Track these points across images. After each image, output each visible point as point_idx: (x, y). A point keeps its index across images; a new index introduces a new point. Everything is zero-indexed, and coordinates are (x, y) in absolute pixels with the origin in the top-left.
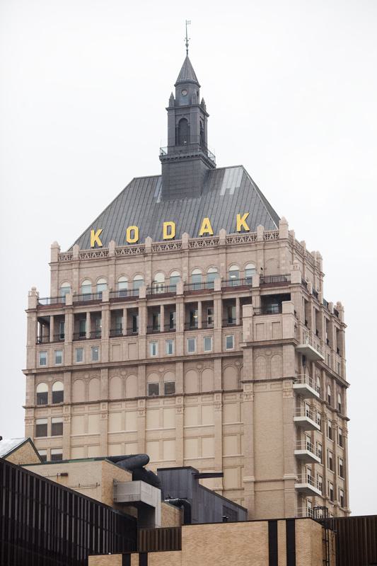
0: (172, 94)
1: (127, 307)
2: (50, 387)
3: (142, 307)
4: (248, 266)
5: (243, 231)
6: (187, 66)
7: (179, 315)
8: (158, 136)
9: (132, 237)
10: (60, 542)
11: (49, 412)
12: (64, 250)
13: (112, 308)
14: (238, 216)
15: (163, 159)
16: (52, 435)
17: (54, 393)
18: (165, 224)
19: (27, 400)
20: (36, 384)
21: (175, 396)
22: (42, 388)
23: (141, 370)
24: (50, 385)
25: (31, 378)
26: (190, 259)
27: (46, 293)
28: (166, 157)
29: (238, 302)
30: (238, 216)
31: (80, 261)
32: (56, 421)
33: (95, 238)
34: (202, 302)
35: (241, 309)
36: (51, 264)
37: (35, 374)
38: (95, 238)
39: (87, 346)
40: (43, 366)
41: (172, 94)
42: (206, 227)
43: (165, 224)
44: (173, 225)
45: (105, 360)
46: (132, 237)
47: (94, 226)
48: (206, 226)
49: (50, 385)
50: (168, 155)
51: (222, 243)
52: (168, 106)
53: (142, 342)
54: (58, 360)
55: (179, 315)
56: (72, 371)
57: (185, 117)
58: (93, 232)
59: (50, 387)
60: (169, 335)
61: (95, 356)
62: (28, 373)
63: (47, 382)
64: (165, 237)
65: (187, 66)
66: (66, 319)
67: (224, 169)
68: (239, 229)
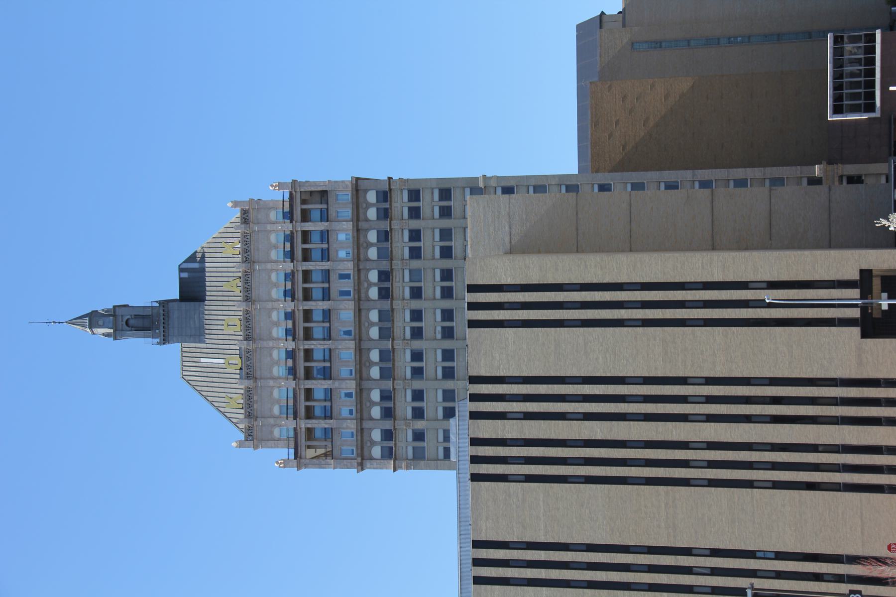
1: (303, 440)
2: (375, 404)
6: (76, 321)
8: (141, 347)
11: (398, 324)
13: (299, 218)
15: (165, 341)
16: (423, 400)
17: (380, 279)
21: (393, 310)
22: (376, 451)
23: (367, 424)
24: (373, 443)
25: (368, 463)
27: (284, 453)
29: (307, 325)
31: (255, 379)
32: (408, 358)
35: (315, 361)
36: (255, 447)
37: (362, 460)
40: (353, 333)
45: (350, 265)
53: (335, 226)
54: (349, 395)
56: (362, 419)
57: (125, 320)
59: (375, 404)
62: (361, 467)
63: (370, 408)
65: (76, 321)
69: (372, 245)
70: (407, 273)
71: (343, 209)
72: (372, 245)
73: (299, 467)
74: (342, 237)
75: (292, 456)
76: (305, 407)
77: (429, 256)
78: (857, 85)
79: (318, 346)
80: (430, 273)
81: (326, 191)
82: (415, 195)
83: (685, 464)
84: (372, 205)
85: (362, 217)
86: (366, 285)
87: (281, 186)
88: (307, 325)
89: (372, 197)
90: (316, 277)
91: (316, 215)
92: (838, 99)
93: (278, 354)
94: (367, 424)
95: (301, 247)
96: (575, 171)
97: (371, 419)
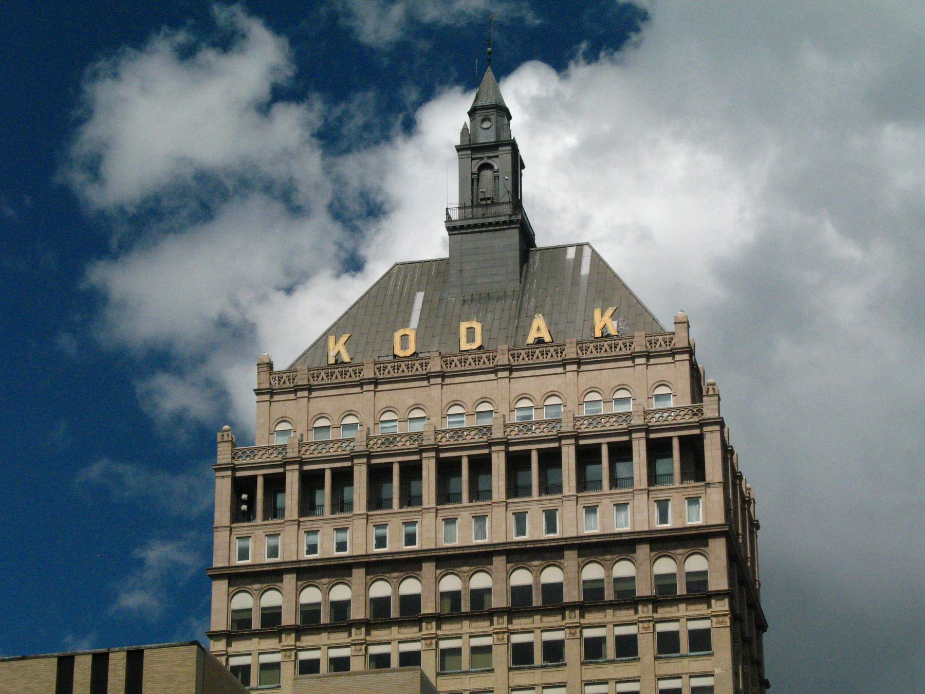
0: (465, 124)
3: (429, 458)
5: (338, 363)
7: (291, 498)
14: (597, 313)
15: (453, 229)
18: (464, 326)
26: (377, 394)
28: (458, 224)
30: (597, 313)
34: (610, 444)
39: (535, 508)
41: (465, 124)
42: (538, 329)
44: (478, 327)
47: (336, 329)
48: (539, 328)
50: (460, 220)
52: (458, 143)
55: (291, 498)
57: (490, 161)
58: (332, 340)
61: (410, 539)
64: (464, 346)
66: (356, 474)
68: (598, 334)
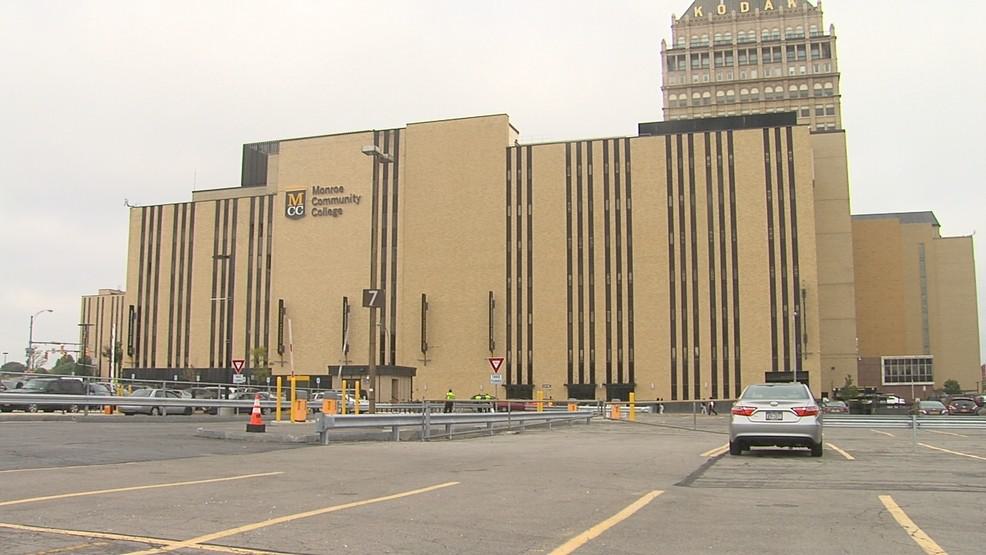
4: (798, 28)
9: (722, 11)
10: (378, 427)
12: (678, 18)
14: (795, 5)
18: (742, 4)
19: (664, 116)
20: (669, 95)
22: (673, 97)
23: (689, 91)
24: (678, 96)
29: (700, 56)
33: (698, 11)
38: (698, 11)
43: (742, 4)
44: (747, 4)
46: (722, 11)
49: (678, 96)
51: (782, 13)
60: (827, 61)
67: (278, 142)
69: (799, 88)
70: (831, 106)
71: (822, 69)
72: (799, 88)
73: (662, 53)
74: (803, 69)
75: (668, 48)
76: (698, 53)
77: (819, 121)
78: (922, 372)
79: (710, 61)
80: (832, 120)
81: (830, 57)
82: (831, 112)
83: (619, 270)
84: (823, 86)
85: (743, 86)
86: (749, 87)
87: (832, 27)
88: (700, 56)
89: (828, 86)
90: (753, 57)
91: (816, 52)
92: (895, 362)
93: (799, 30)
94: (689, 91)
95: (795, 45)
96: (857, 208)
97: (692, 93)
